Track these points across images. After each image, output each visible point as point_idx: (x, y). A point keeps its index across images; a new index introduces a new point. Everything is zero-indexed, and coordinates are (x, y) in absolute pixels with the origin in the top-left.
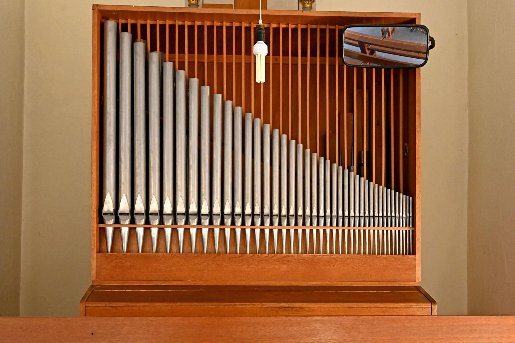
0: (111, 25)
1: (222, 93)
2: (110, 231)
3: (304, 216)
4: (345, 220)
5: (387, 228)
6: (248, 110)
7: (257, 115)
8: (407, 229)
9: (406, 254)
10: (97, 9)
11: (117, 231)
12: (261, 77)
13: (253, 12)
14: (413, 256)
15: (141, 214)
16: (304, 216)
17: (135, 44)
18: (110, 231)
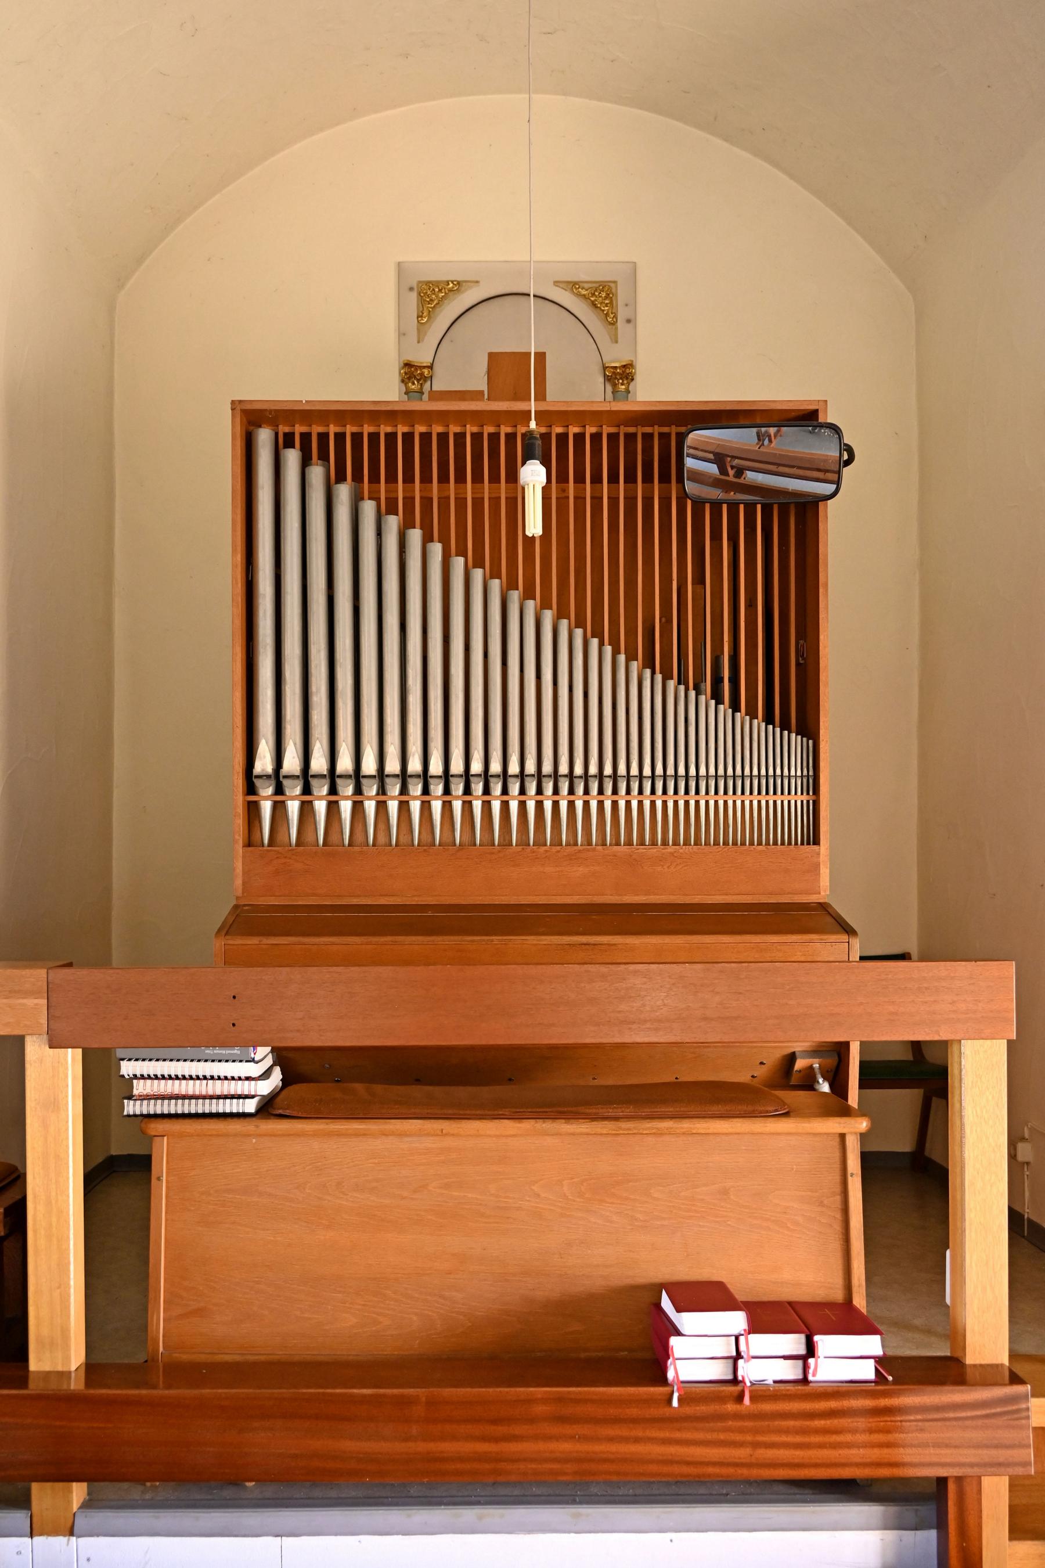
0: (264, 437)
1: (464, 555)
2: (266, 807)
3: (615, 776)
4: (691, 783)
5: (768, 798)
6: (512, 585)
7: (529, 594)
8: (805, 798)
9: (802, 844)
10: (238, 408)
11: (279, 808)
12: (534, 526)
13: (519, 406)
14: (816, 847)
15: (323, 776)
16: (615, 776)
17: (307, 469)
18: (266, 807)
